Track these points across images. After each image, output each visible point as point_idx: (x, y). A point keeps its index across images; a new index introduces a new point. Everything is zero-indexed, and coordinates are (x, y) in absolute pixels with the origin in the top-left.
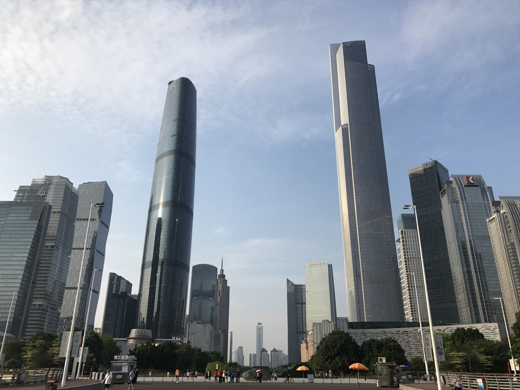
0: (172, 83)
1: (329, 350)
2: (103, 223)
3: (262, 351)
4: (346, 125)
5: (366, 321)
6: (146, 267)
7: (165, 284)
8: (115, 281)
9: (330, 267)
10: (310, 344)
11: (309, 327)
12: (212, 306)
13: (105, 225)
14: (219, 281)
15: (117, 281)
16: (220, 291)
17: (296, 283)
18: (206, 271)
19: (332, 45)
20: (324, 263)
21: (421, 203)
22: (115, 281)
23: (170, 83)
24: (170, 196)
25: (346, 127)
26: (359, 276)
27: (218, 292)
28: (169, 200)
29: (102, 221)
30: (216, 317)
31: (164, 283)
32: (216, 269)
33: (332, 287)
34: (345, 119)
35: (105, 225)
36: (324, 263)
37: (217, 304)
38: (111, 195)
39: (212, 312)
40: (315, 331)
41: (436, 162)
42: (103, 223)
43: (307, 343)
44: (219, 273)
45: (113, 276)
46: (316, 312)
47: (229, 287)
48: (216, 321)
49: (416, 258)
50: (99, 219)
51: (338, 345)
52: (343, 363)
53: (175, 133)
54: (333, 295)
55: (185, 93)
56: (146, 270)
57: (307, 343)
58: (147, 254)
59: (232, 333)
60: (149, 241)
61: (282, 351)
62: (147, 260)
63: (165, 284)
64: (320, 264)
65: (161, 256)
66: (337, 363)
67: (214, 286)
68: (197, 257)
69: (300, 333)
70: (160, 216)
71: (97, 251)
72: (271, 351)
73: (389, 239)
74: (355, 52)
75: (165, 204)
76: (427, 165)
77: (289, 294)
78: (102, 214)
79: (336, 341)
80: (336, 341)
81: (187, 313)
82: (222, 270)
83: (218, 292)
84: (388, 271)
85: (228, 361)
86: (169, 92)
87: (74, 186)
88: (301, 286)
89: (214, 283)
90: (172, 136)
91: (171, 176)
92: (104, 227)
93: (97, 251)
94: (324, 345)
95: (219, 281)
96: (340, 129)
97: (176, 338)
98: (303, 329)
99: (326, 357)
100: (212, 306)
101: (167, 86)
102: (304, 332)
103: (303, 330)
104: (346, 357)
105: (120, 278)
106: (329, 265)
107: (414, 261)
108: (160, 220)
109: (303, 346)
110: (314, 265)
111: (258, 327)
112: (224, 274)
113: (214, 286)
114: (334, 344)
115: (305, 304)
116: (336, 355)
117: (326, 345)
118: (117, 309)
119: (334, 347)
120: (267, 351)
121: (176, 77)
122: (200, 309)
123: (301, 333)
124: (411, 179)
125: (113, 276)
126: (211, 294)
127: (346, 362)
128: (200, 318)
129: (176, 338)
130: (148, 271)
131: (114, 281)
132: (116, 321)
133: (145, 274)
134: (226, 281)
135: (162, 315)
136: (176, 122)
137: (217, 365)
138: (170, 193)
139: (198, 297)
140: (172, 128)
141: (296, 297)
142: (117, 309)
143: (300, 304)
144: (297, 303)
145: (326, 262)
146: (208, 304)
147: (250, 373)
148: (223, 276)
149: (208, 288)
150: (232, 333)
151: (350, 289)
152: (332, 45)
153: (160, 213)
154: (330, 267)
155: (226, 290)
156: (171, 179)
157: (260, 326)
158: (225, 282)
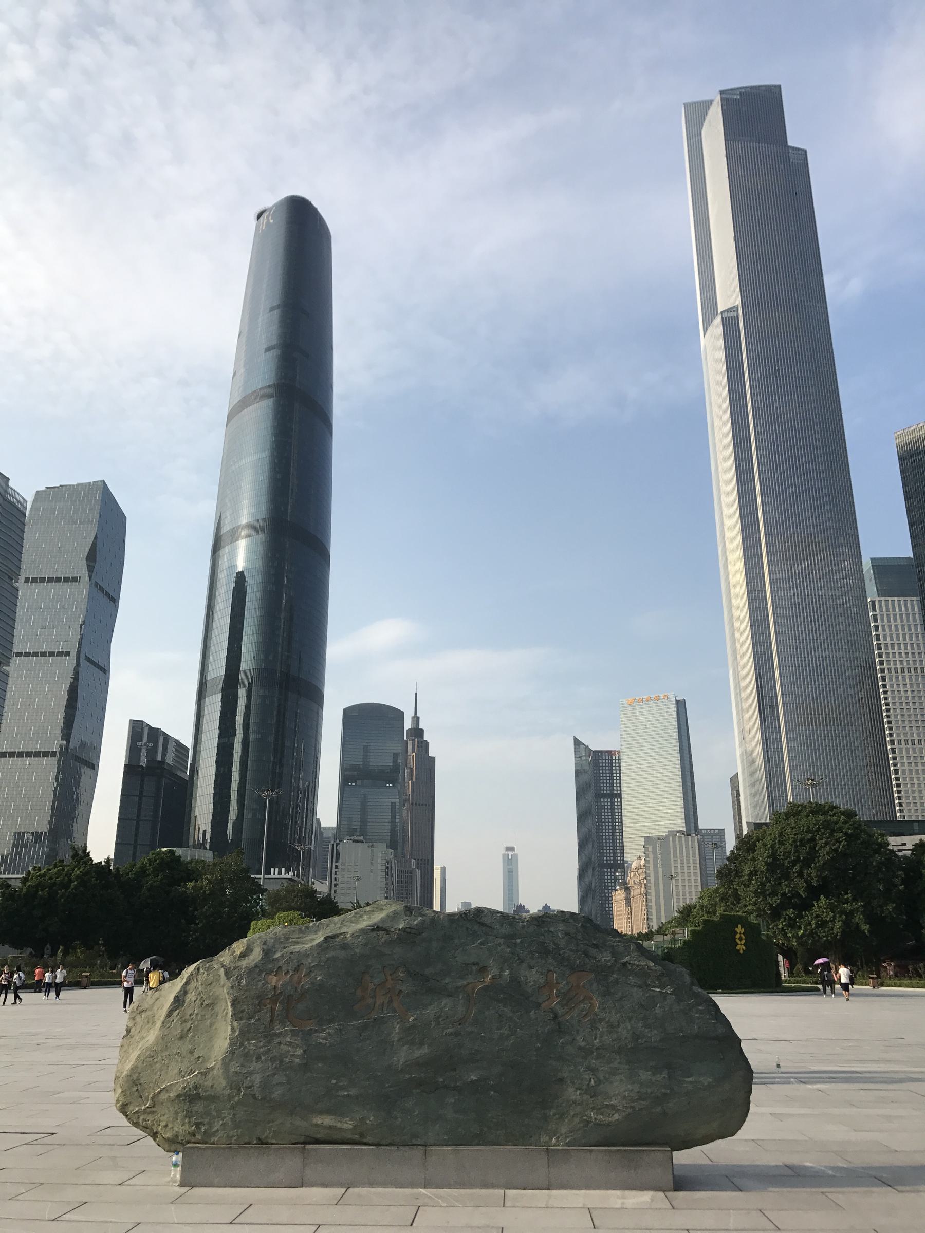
0: (265, 215)
1: (786, 876)
2: (101, 589)
7: (259, 736)
8: (145, 740)
9: (681, 706)
10: (635, 892)
11: (633, 852)
12: (393, 804)
13: (107, 594)
15: (148, 741)
16: (411, 769)
17: (596, 744)
18: (371, 723)
20: (666, 697)
22: (145, 740)
23: (259, 216)
24: (264, 508)
25: (735, 314)
26: (772, 707)
28: (263, 515)
29: (96, 584)
30: (404, 831)
31: (254, 732)
32: (400, 715)
33: (686, 752)
34: (729, 294)
35: (107, 594)
36: (666, 697)
37: (405, 801)
38: (121, 520)
39: (393, 817)
42: (101, 589)
43: (627, 889)
44: (408, 725)
45: (138, 730)
46: (648, 811)
48: (404, 841)
49: (909, 670)
50: (90, 577)
51: (824, 854)
52: (846, 923)
53: (274, 342)
55: (300, 241)
56: (208, 701)
57: (627, 889)
58: (211, 659)
59: (443, 870)
60: (214, 632)
64: (657, 699)
65: (247, 662)
66: (823, 924)
67: (396, 756)
69: (610, 866)
70: (241, 565)
71: (89, 660)
73: (854, 611)
74: (755, 118)
75: (254, 528)
77: (578, 774)
78: (97, 566)
79: (813, 839)
80: (813, 839)
82: (416, 719)
83: (407, 771)
84: (851, 692)
86: (260, 238)
87: (11, 484)
88: (610, 753)
89: (398, 748)
91: (266, 454)
92: (106, 600)
93: (89, 660)
94: (762, 855)
96: (717, 323)
97: (280, 873)
98: (615, 857)
99: (775, 901)
100: (393, 804)
101: (254, 223)
102: (620, 864)
103: (615, 860)
104: (855, 899)
105: (155, 733)
106: (678, 702)
107: (904, 677)
108: (240, 578)
109: (618, 896)
110: (641, 700)
111: (506, 857)
112: (421, 727)
113: (396, 756)
114: (806, 850)
116: (814, 893)
117: (773, 855)
118: (140, 804)
119: (807, 863)
121: (272, 199)
123: (610, 866)
124: (901, 459)
125: (138, 730)
127: (858, 918)
128: (363, 832)
129: (280, 873)
130: (214, 704)
132: (136, 835)
133: (206, 710)
134: (427, 743)
135: (250, 816)
136: (276, 313)
137: (741, 948)
138: (264, 499)
139: (359, 783)
140: (268, 330)
141: (598, 784)
142: (140, 804)
143: (605, 796)
144: (599, 796)
145: (672, 695)
146: (385, 798)
147: (264, 1007)
148: (417, 732)
149: (381, 760)
150: (443, 870)
151: (748, 744)
153: (242, 555)
154: (681, 706)
155: (427, 766)
156: (266, 462)
157: (510, 853)
158: (425, 746)
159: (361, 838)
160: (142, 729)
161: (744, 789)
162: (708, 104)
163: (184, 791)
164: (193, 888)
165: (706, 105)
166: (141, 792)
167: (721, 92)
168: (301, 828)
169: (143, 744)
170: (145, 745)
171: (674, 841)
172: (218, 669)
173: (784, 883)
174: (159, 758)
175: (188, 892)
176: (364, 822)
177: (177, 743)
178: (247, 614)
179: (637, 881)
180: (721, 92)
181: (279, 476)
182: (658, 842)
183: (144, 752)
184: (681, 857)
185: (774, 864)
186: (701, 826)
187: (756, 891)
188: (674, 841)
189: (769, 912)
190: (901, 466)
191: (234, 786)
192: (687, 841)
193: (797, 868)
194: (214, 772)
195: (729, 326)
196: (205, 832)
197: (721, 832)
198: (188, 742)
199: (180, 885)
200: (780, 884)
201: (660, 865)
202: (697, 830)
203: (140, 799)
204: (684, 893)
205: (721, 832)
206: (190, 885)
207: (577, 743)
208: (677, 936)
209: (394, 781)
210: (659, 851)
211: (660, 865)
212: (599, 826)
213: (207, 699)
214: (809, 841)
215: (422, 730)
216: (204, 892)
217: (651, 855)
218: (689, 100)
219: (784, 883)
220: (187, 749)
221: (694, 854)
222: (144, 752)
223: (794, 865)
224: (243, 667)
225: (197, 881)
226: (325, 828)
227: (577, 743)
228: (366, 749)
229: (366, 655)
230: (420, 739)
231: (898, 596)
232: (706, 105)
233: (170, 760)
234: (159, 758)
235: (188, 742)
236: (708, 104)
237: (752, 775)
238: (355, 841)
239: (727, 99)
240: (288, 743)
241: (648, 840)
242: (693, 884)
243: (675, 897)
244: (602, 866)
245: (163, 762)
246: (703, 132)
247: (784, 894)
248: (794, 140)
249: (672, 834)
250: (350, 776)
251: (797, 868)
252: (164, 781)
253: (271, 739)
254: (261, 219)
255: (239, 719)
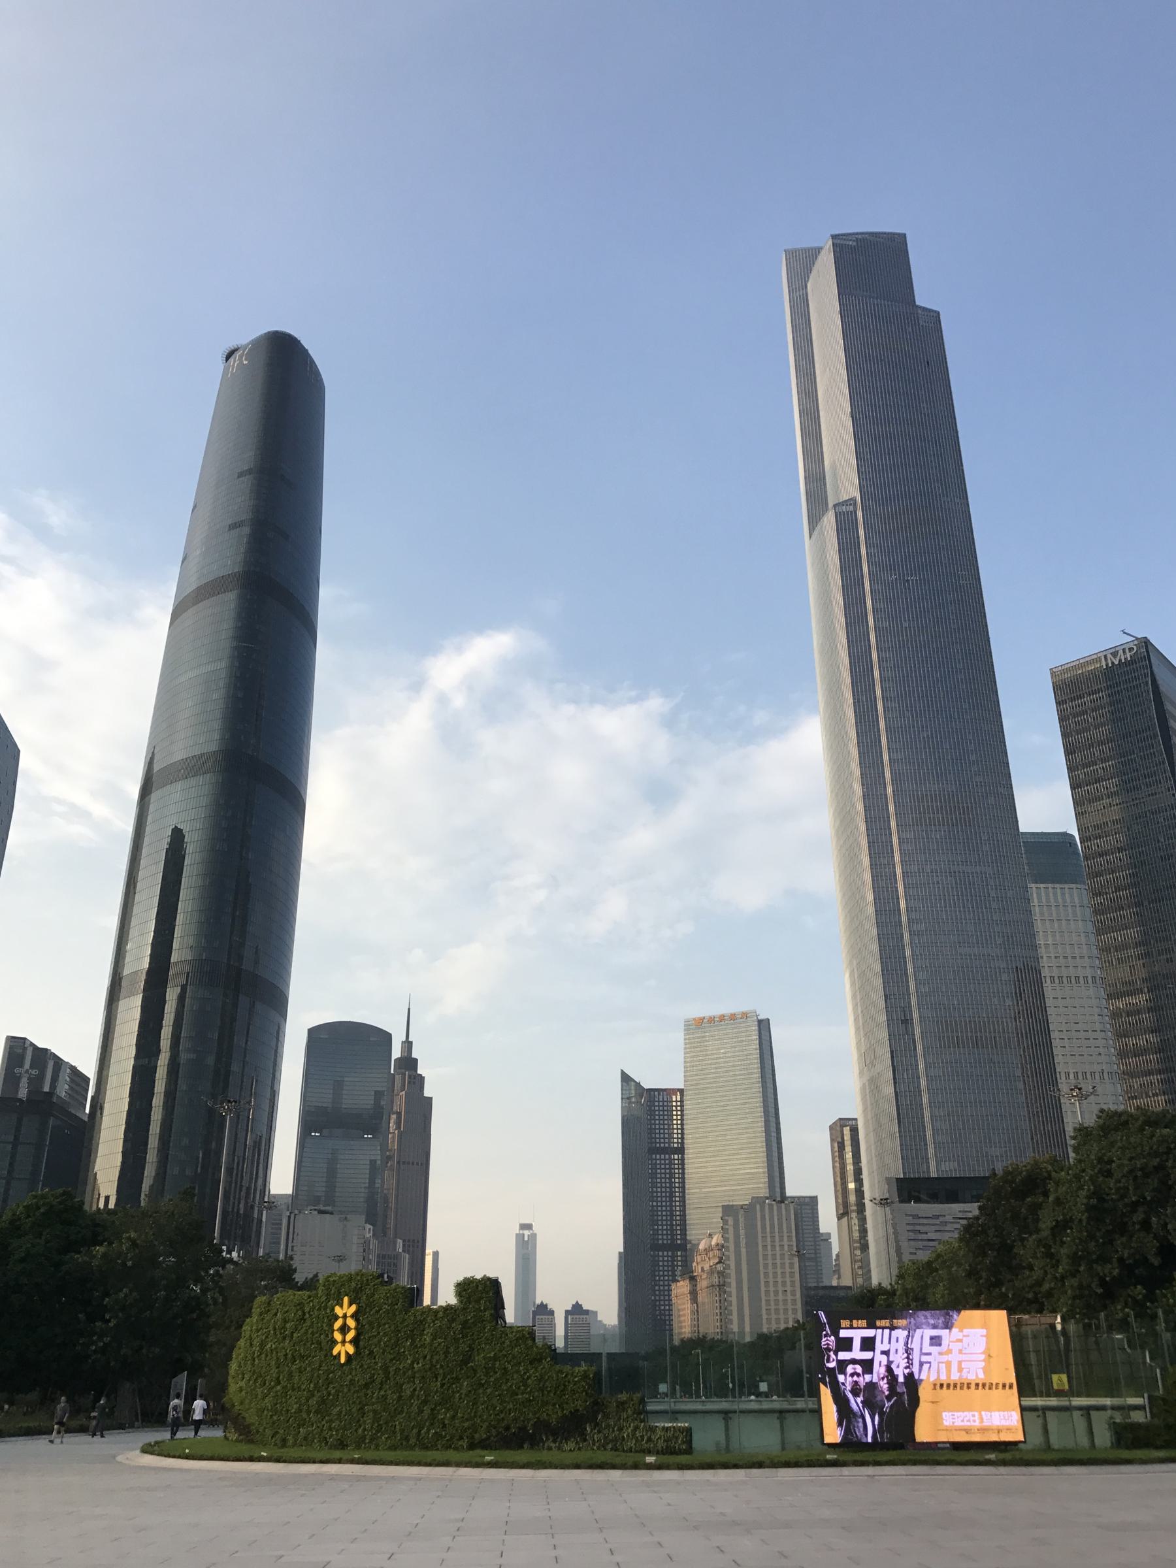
3: (535, 1313)
4: (852, 502)
5: (934, 1175)
6: (123, 991)
7: (192, 1056)
8: (27, 1065)
10: (703, 1283)
14: (398, 1078)
15: (31, 1067)
16: (399, 1114)
18: (347, 1047)
19: (791, 255)
21: (1098, 780)
22: (27, 1065)
23: (229, 356)
25: (851, 509)
27: (394, 1117)
28: (213, 747)
30: (386, 1200)
32: (387, 1037)
34: (845, 484)
39: (372, 1181)
40: (731, 1236)
41: (1146, 642)
44: (396, 1053)
46: (718, 1171)
47: (431, 1099)
54: (773, 1120)
56: (122, 1005)
57: (693, 1279)
59: (436, 1255)
61: (595, 1313)
62: (127, 970)
63: (192, 1056)
65: (179, 953)
67: (378, 1095)
68: (317, 993)
72: (567, 1313)
76: (1115, 654)
79: (1160, 1168)
81: (281, 1179)
82: (408, 1045)
83: (394, 1117)
85: (427, 1301)
90: (232, 527)
95: (398, 1078)
96: (829, 521)
101: (220, 365)
105: (43, 1056)
109: (681, 1288)
111: (520, 1237)
112: (414, 1055)
113: (378, 1095)
115: (681, 1150)
117: (1098, 1194)
120: (552, 1313)
121: (249, 330)
122: (332, 1174)
126: (370, 1122)
130: (131, 1009)
131: (21, 1066)
133: (120, 1018)
134: (421, 1079)
136: (247, 481)
139: (326, 1132)
141: (651, 1132)
146: (358, 1157)
148: (409, 1063)
150: (436, 1255)
152: (791, 255)
155: (421, 1110)
157: (527, 1233)
159: (329, 1208)
160: (25, 1049)
161: (867, 1135)
162: (816, 252)
163: (82, 1136)
164: (104, 1255)
165: (813, 254)
166: (16, 1138)
167: (834, 237)
168: (248, 1193)
169: (23, 1070)
170: (27, 1072)
171: (762, 1210)
172: (140, 959)
173: (1120, 1241)
174: (46, 1089)
175: (95, 1263)
176: (331, 1186)
177: (74, 1069)
178: (184, 882)
179: (707, 1267)
180: (834, 237)
181: (240, 695)
182: (742, 1212)
183: (24, 1082)
184: (772, 1232)
185: (1099, 1209)
186: (790, 1192)
187: (1076, 1253)
188: (762, 1210)
189: (1100, 1291)
190: (1060, 712)
191: (155, 1128)
192: (779, 1210)
193: (1139, 1216)
194: (126, 1108)
195: (845, 523)
196: (107, 1198)
197: (813, 1201)
198: (89, 1069)
199: (79, 1253)
200: (1111, 1242)
201: (743, 1244)
202: (784, 1198)
203: (15, 1147)
204: (776, 1283)
205: (813, 1201)
206: (100, 1250)
207: (626, 1078)
208: (1024, 1329)
209: (374, 1130)
210: (742, 1225)
211: (743, 1244)
212: (652, 1192)
213: (121, 1003)
214: (1157, 1169)
215: (416, 1060)
216: (124, 1264)
217: (731, 1230)
218: (789, 247)
219: (1120, 1241)
220: (87, 1080)
221: (789, 1228)
222: (24, 1082)
223: (1134, 1211)
224: (174, 958)
225: (110, 1244)
226: (275, 1196)
227: (626, 1078)
228: (338, 1085)
229: (339, 963)
230: (412, 1073)
231: (1053, 882)
232: (813, 254)
233: (63, 1090)
234: (46, 1089)
235: (89, 1069)
236: (816, 252)
237: (865, 1116)
238: (321, 1212)
239: (841, 246)
240: (235, 1067)
241: (728, 1210)
242: (788, 1270)
243: (763, 1289)
244: (656, 1247)
245: (50, 1094)
246: (809, 285)
247: (1121, 1260)
248: (923, 298)
249: (756, 1200)
250: (310, 1122)
251: (1139, 1216)
252: (51, 1121)
253: (211, 1060)
254: (232, 360)
255: (166, 1033)
